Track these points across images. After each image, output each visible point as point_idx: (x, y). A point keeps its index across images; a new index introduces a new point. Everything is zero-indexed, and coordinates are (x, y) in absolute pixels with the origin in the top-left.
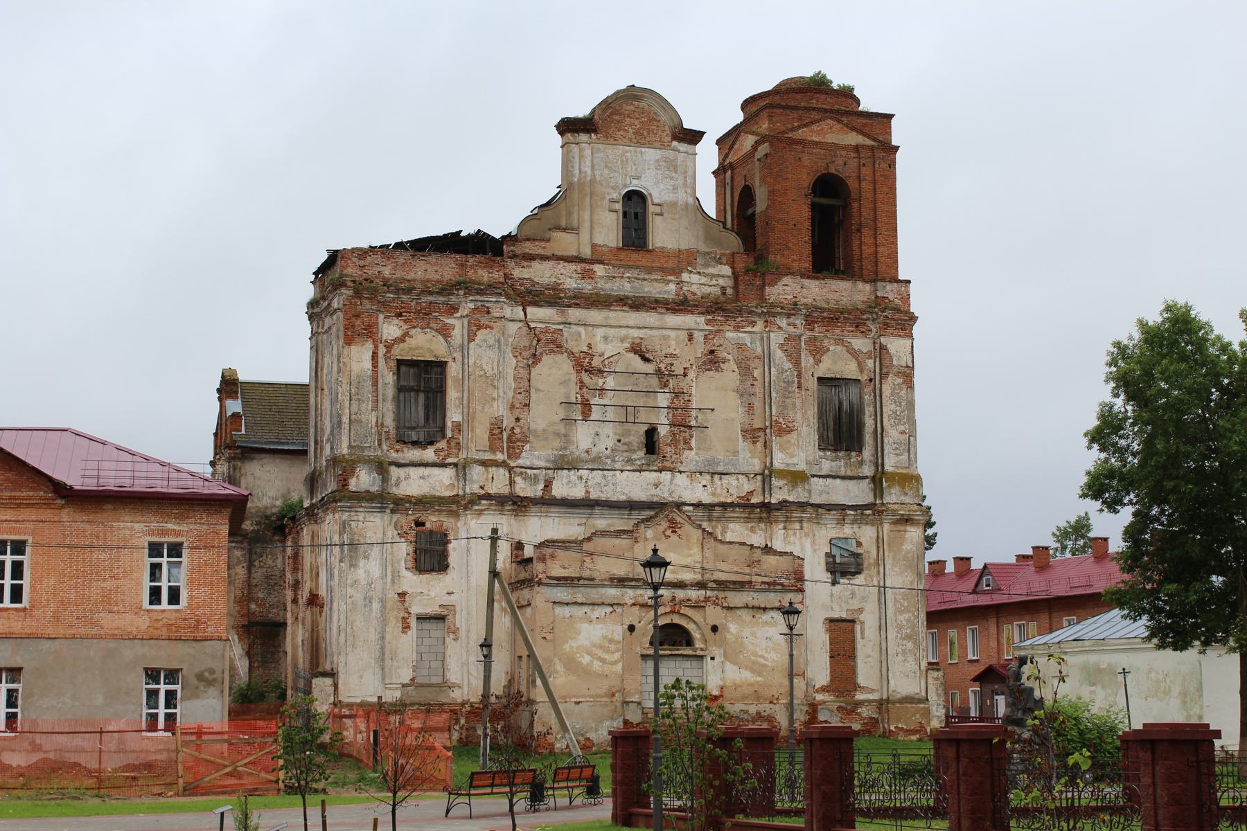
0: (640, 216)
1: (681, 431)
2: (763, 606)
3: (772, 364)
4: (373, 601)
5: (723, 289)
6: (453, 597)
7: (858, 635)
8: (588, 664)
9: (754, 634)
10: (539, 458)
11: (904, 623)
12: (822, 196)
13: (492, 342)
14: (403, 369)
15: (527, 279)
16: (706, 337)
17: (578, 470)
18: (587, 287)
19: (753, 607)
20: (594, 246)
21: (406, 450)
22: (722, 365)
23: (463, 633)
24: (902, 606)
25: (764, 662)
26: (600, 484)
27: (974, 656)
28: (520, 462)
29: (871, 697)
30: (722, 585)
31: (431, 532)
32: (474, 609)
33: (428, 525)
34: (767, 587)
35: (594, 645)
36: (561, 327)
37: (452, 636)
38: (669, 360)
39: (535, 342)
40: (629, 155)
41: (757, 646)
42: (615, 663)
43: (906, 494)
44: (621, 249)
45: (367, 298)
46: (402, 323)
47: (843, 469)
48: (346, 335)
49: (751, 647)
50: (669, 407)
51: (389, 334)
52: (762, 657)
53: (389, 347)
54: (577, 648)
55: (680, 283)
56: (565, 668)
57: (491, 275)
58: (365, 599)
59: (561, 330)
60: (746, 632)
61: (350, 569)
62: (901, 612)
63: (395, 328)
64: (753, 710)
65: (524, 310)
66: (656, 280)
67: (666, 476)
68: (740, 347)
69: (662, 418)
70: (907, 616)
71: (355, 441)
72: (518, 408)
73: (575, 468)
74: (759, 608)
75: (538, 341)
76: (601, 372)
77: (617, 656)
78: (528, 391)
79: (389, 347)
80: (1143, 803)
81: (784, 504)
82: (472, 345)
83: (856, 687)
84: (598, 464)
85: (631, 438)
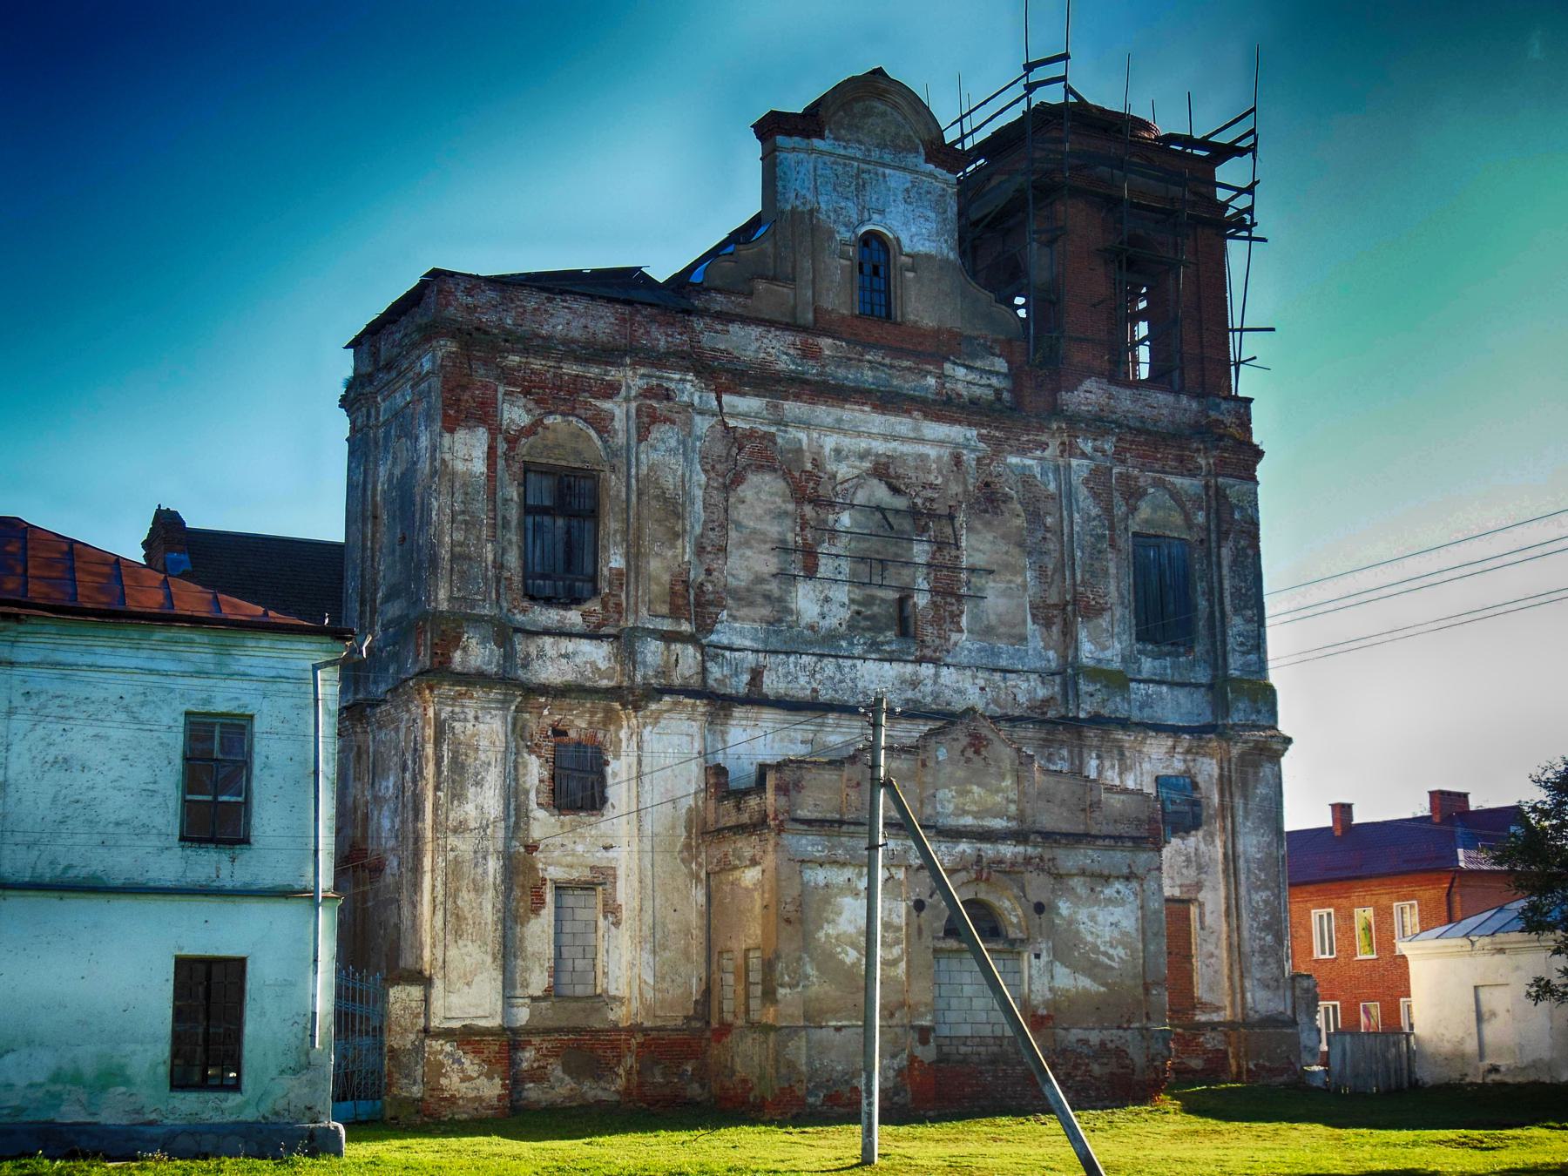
1: (946, 603)
2: (1106, 872)
3: (1075, 507)
4: (489, 858)
5: (998, 392)
6: (611, 854)
7: (1195, 924)
8: (853, 965)
9: (1093, 918)
10: (741, 633)
11: (1261, 905)
13: (673, 443)
14: (532, 477)
15: (722, 351)
16: (979, 460)
17: (801, 654)
18: (812, 370)
19: (1092, 875)
22: (1003, 506)
24: (1258, 879)
25: (1109, 962)
26: (832, 678)
27: (1323, 952)
28: (714, 637)
29: (1215, 1018)
30: (1050, 837)
31: (579, 744)
32: (650, 873)
33: (573, 734)
34: (1112, 842)
36: (773, 429)
38: (929, 493)
39: (735, 450)
40: (865, 176)
41: (1098, 936)
43: (1259, 712)
44: (857, 317)
45: (479, 359)
46: (531, 405)
47: (1169, 671)
48: (446, 415)
49: (1089, 938)
50: (929, 565)
51: (512, 420)
52: (1105, 954)
53: (512, 441)
54: (837, 937)
55: (942, 376)
56: (818, 969)
57: (670, 339)
58: (475, 852)
59: (773, 435)
60: (1082, 915)
61: (452, 803)
62: (1258, 889)
63: (521, 411)
64: (1094, 1037)
67: (927, 670)
68: (1026, 479)
69: (920, 580)
70: (1265, 894)
71: (459, 590)
72: (709, 553)
73: (795, 653)
74: (1101, 876)
75: (740, 450)
76: (832, 504)
78: (724, 527)
79: (512, 441)
81: (1096, 720)
82: (643, 446)
83: (1194, 1004)
84: (826, 644)
85: (876, 609)
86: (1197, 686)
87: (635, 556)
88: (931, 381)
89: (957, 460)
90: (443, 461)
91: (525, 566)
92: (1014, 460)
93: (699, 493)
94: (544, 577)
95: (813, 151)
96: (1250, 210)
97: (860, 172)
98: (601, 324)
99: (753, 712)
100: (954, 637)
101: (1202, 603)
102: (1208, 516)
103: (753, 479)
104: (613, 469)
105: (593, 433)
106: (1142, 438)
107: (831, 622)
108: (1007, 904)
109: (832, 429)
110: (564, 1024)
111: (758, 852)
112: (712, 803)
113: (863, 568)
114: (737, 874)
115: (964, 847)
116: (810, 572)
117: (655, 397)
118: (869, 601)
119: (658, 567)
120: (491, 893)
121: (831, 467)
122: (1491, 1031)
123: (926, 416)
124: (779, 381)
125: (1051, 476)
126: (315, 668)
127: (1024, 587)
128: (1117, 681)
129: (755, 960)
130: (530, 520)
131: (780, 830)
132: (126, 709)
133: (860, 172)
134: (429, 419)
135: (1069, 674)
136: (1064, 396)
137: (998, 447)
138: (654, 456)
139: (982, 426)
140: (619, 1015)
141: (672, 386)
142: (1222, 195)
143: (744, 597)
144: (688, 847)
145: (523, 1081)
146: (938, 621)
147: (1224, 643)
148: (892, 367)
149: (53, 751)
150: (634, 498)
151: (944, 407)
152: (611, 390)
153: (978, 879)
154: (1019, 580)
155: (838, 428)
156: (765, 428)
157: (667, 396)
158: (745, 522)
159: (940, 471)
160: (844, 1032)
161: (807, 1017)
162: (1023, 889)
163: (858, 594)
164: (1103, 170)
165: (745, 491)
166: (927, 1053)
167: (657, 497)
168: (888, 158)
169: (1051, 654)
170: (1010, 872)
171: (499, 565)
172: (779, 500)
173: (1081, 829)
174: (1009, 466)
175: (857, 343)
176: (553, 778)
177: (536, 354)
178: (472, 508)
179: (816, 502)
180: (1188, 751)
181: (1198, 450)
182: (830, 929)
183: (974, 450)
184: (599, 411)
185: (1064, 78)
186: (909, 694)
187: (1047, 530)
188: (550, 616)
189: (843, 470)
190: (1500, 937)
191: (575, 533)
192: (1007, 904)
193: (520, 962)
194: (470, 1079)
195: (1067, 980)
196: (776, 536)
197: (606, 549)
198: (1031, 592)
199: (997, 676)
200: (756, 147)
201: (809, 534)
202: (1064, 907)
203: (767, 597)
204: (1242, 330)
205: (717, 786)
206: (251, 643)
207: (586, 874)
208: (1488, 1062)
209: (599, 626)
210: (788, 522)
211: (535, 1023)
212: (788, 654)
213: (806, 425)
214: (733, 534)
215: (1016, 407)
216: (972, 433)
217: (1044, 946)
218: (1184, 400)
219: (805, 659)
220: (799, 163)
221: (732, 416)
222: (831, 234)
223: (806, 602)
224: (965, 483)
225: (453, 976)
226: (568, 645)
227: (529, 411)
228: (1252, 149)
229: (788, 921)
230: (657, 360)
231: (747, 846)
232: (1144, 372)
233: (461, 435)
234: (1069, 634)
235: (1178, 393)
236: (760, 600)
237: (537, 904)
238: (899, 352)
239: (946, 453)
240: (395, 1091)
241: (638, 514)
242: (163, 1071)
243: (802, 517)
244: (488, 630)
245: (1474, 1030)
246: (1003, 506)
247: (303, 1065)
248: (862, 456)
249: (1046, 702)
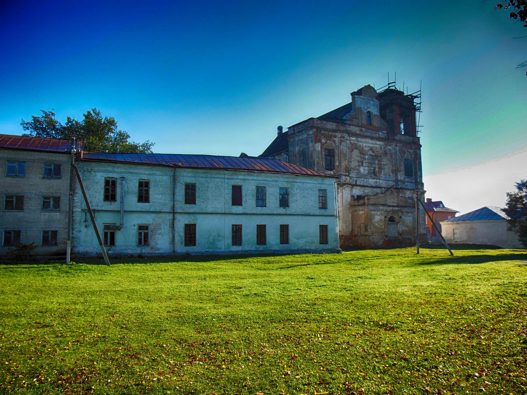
5: (385, 136)
9: (407, 219)
10: (354, 175)
13: (345, 145)
16: (384, 147)
18: (362, 134)
30: (402, 206)
35: (378, 221)
36: (357, 143)
38: (377, 153)
42: (382, 226)
50: (378, 164)
53: (323, 145)
55: (379, 134)
60: (406, 218)
64: (407, 237)
67: (378, 180)
68: (390, 150)
76: (365, 154)
77: (383, 224)
81: (401, 188)
84: (364, 176)
86: (413, 183)
87: (340, 163)
88: (377, 135)
89: (381, 147)
90: (315, 148)
91: (326, 164)
92: (388, 147)
95: (360, 98)
96: (420, 107)
99: (356, 187)
100: (381, 175)
101: (414, 170)
102: (414, 156)
105: (333, 143)
107: (365, 173)
108: (396, 217)
111: (363, 209)
112: (353, 201)
113: (369, 165)
114: (358, 212)
115: (391, 208)
116: (362, 165)
118: (370, 170)
119: (343, 164)
121: (365, 148)
122: (456, 236)
124: (358, 135)
126: (335, 183)
128: (403, 182)
129: (362, 225)
131: (368, 205)
132: (311, 189)
133: (367, 101)
134: (312, 141)
135: (397, 181)
136: (395, 137)
138: (343, 147)
141: (344, 136)
142: (415, 104)
143: (354, 169)
144: (349, 208)
146: (379, 173)
147: (417, 176)
149: (303, 195)
150: (340, 154)
151: (379, 139)
152: (335, 137)
153: (393, 213)
155: (365, 142)
157: (344, 137)
160: (376, 236)
162: (398, 214)
163: (369, 169)
164: (399, 100)
165: (353, 152)
166: (387, 239)
170: (396, 211)
173: (405, 205)
174: (388, 148)
179: (363, 154)
180: (412, 193)
182: (374, 221)
184: (334, 140)
185: (395, 86)
186: (376, 184)
189: (366, 149)
190: (458, 222)
192: (396, 217)
195: (404, 228)
196: (358, 160)
197: (336, 162)
199: (387, 181)
200: (351, 97)
201: (362, 159)
202: (403, 217)
203: (357, 169)
204: (418, 126)
205: (353, 198)
206: (326, 179)
208: (455, 241)
209: (335, 174)
212: (360, 178)
213: (361, 142)
215: (388, 139)
216: (383, 143)
217: (401, 223)
219: (362, 179)
220: (358, 100)
221: (352, 141)
223: (362, 169)
228: (420, 97)
230: (343, 132)
231: (361, 208)
232: (403, 133)
233: (317, 144)
234: (396, 175)
235: (410, 136)
238: (373, 130)
241: (341, 157)
242: (319, 241)
245: (453, 235)
247: (336, 241)
249: (394, 185)
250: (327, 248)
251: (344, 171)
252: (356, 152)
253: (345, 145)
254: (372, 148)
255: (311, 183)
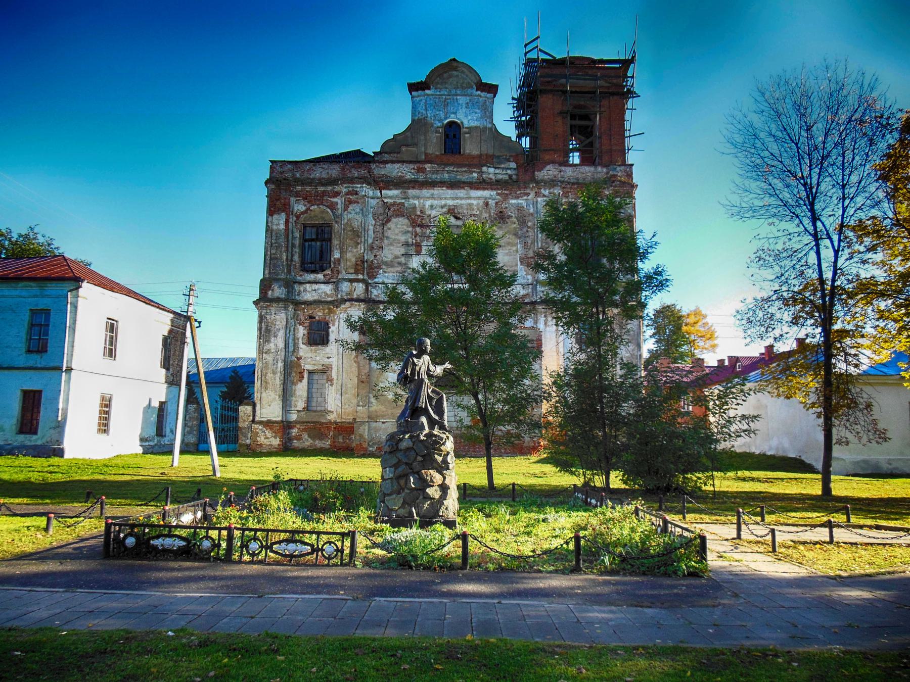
0: (457, 136)
6: (330, 360)
10: (388, 278)
12: (587, 127)
13: (358, 210)
16: (496, 203)
18: (421, 177)
20: (426, 154)
21: (306, 274)
22: (507, 220)
23: (335, 381)
28: (376, 280)
31: (319, 321)
33: (317, 318)
36: (403, 201)
37: (329, 383)
39: (387, 210)
46: (306, 203)
53: (298, 217)
65: (381, 192)
66: (465, 171)
68: (519, 208)
79: (298, 217)
80: (603, 345)
92: (513, 201)
93: (371, 228)
94: (311, 263)
95: (428, 95)
97: (446, 99)
98: (334, 171)
103: (394, 220)
104: (337, 222)
105: (329, 210)
106: (575, 187)
109: (429, 198)
110: (310, 420)
117: (352, 194)
119: (351, 256)
120: (279, 374)
121: (428, 212)
123: (471, 188)
125: (531, 206)
127: (517, 251)
130: (307, 244)
136: (536, 173)
137: (506, 197)
138: (350, 216)
139: (498, 189)
140: (332, 417)
141: (358, 189)
143: (390, 265)
145: (293, 440)
148: (457, 171)
152: (337, 194)
154: (514, 248)
155: (432, 197)
156: (400, 201)
157: (356, 193)
158: (391, 236)
159: (478, 209)
161: (369, 417)
167: (350, 231)
168: (459, 92)
169: (529, 277)
171: (290, 260)
172: (405, 227)
174: (511, 204)
175: (441, 165)
176: (308, 333)
177: (306, 185)
178: (279, 241)
179: (421, 226)
181: (604, 188)
183: (494, 199)
184: (332, 202)
185: (537, 47)
187: (529, 227)
188: (312, 277)
191: (324, 246)
193: (294, 398)
194: (268, 438)
198: (520, 253)
201: (418, 239)
203: (400, 264)
204: (630, 137)
206: (49, 285)
207: (320, 367)
209: (330, 279)
210: (409, 235)
211: (299, 420)
213: (418, 198)
214: (386, 241)
216: (494, 193)
218: (599, 169)
221: (385, 198)
222: (432, 125)
224: (490, 213)
225: (264, 403)
226: (315, 286)
227: (305, 205)
229: (363, 382)
230: (352, 181)
233: (275, 216)
236: (396, 265)
237: (301, 378)
239: (481, 202)
240: (240, 441)
243: (416, 232)
244: (282, 283)
246: (507, 220)
248: (442, 207)
250: (33, 443)
251: (352, 271)
252: (398, 228)
253: (358, 210)
254: (453, 210)
255: (12, 297)
